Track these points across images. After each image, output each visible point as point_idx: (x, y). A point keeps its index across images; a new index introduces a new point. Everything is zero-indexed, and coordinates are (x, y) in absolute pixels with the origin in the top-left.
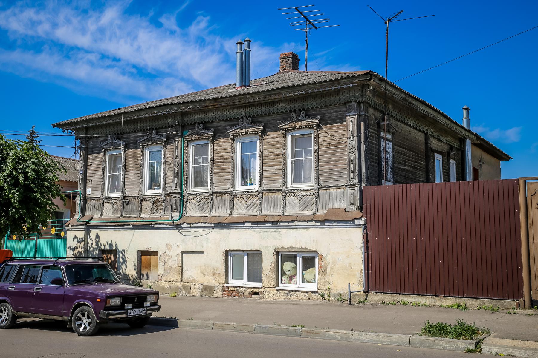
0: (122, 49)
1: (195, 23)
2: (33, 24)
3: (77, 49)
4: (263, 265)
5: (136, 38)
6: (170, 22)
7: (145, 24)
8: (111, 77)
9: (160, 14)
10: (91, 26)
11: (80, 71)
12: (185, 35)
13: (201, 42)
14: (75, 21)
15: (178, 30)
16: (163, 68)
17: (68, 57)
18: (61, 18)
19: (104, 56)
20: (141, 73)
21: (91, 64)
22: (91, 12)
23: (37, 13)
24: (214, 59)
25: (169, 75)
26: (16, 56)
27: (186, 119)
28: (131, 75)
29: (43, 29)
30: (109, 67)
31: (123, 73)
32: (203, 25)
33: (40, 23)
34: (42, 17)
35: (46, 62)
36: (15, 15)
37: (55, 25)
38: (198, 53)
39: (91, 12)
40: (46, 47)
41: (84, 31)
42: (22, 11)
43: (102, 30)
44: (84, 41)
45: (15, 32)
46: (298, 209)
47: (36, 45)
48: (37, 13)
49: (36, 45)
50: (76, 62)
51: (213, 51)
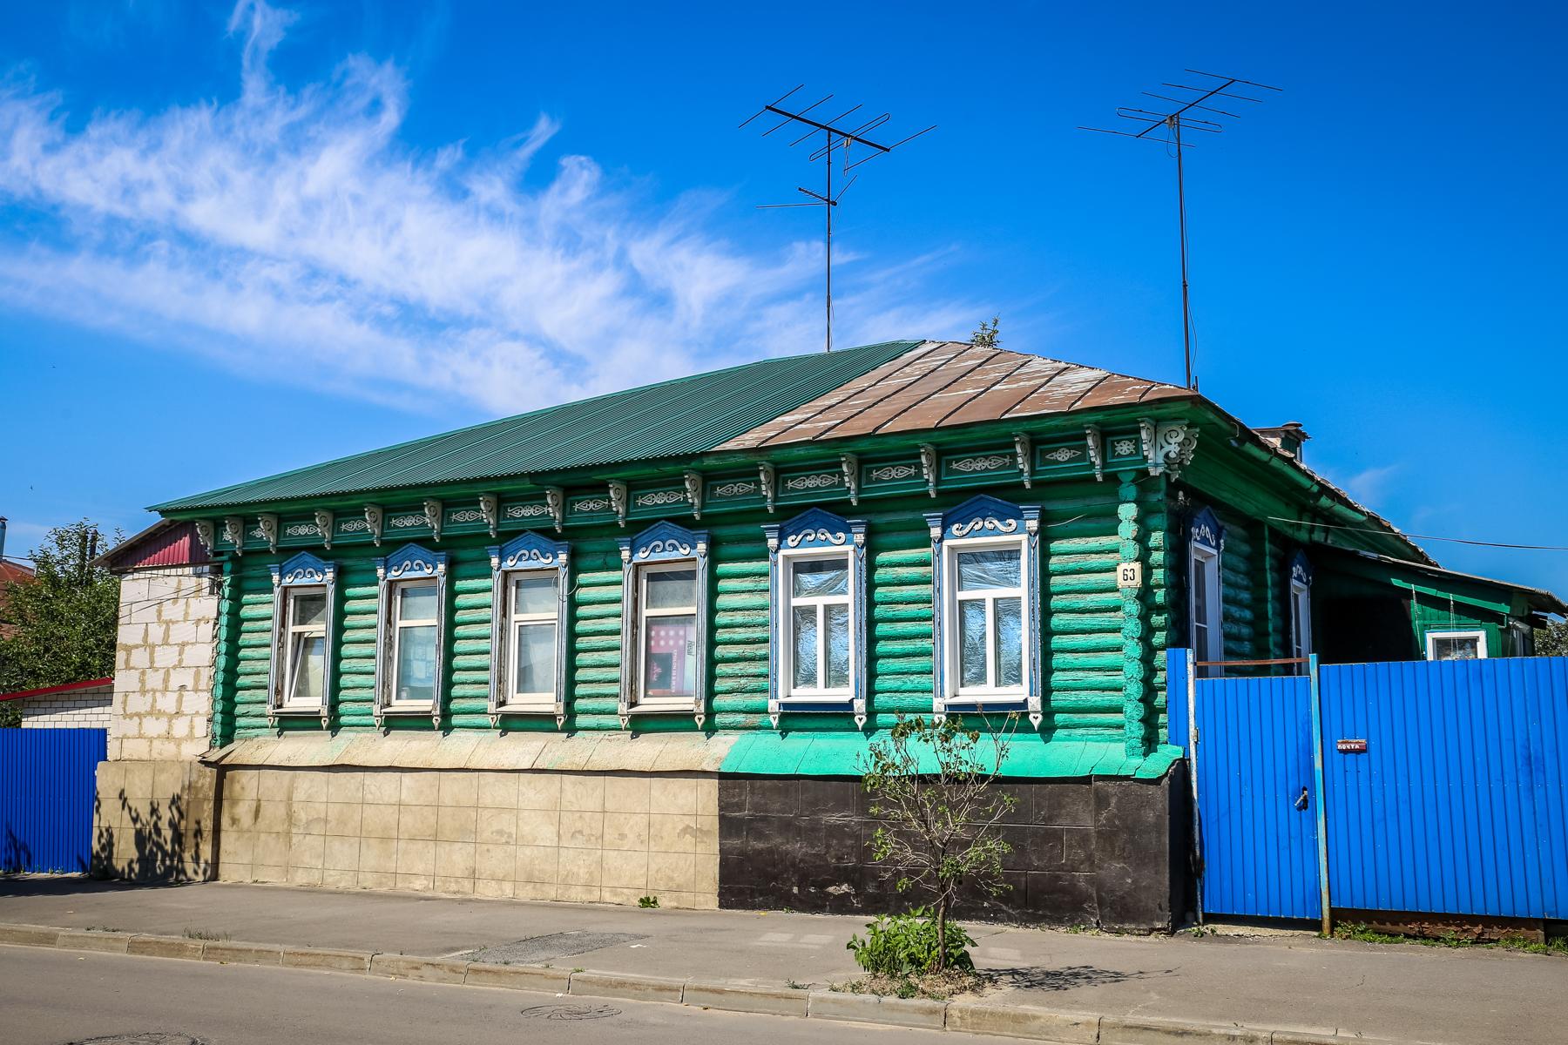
0: (361, 254)
1: (556, 187)
2: (128, 191)
3: (241, 254)
4: (98, 784)
5: (397, 226)
6: (492, 188)
7: (422, 190)
8: (326, 327)
9: (464, 166)
10: (284, 195)
11: (244, 313)
12: (530, 222)
13: (569, 241)
14: (242, 180)
15: (510, 207)
16: (468, 307)
17: (216, 275)
18: (202, 175)
19: (313, 273)
20: (418, 320)
21: (277, 293)
22: (283, 157)
23: (144, 155)
24: (607, 283)
25: (483, 324)
26: (79, 271)
27: (836, 480)
28: (383, 323)
29: (157, 202)
30: (327, 299)
31: (359, 318)
32: (577, 194)
33: (150, 186)
34: (152, 169)
35: (156, 290)
36: (82, 162)
37: (184, 193)
38: (559, 268)
39: (283, 157)
40: (162, 245)
41: (260, 209)
42: (101, 154)
43: (310, 207)
44: (257, 233)
45: (85, 210)
46: (1131, 752)
47: (126, 240)
48: (144, 155)
49: (126, 240)
50: (235, 288)
51: (598, 267)
